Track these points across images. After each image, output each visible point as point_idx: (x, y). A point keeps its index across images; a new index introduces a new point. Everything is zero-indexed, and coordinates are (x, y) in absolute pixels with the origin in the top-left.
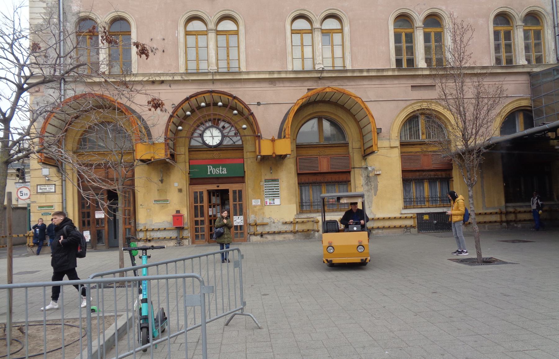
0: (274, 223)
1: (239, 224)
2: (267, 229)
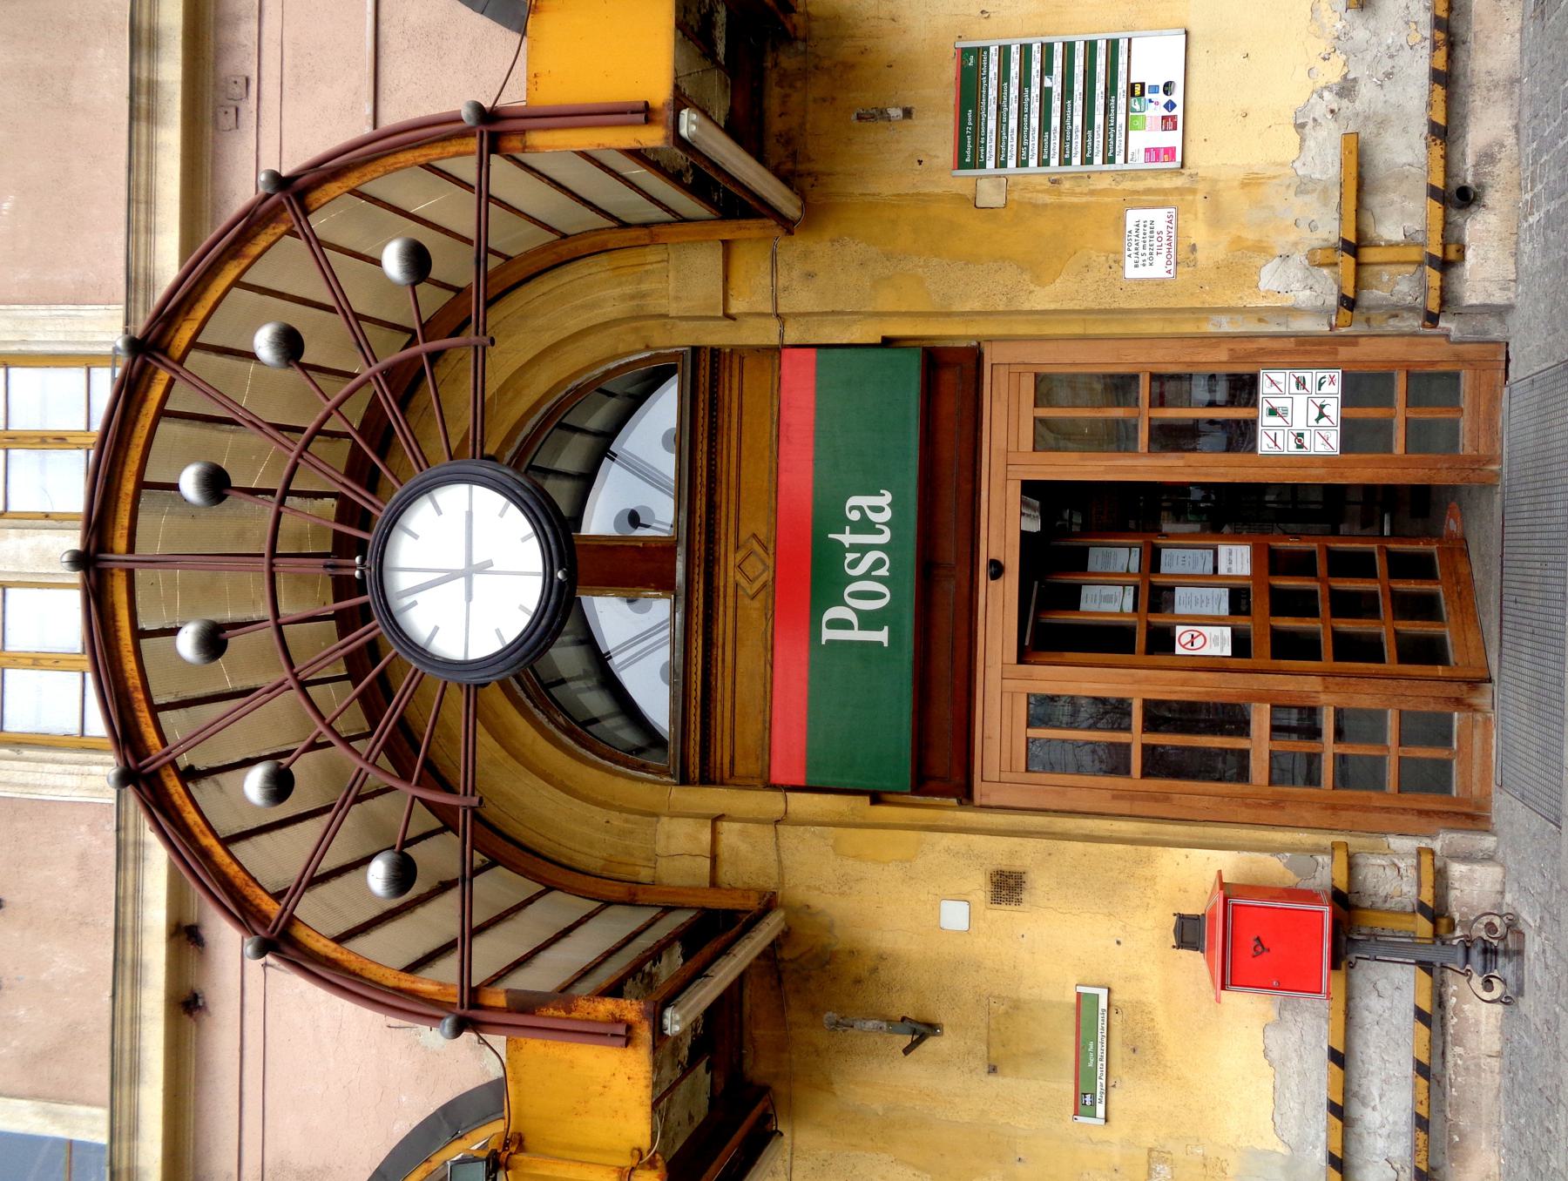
0: (1346, 89)
1: (1333, 410)
2: (1405, 151)
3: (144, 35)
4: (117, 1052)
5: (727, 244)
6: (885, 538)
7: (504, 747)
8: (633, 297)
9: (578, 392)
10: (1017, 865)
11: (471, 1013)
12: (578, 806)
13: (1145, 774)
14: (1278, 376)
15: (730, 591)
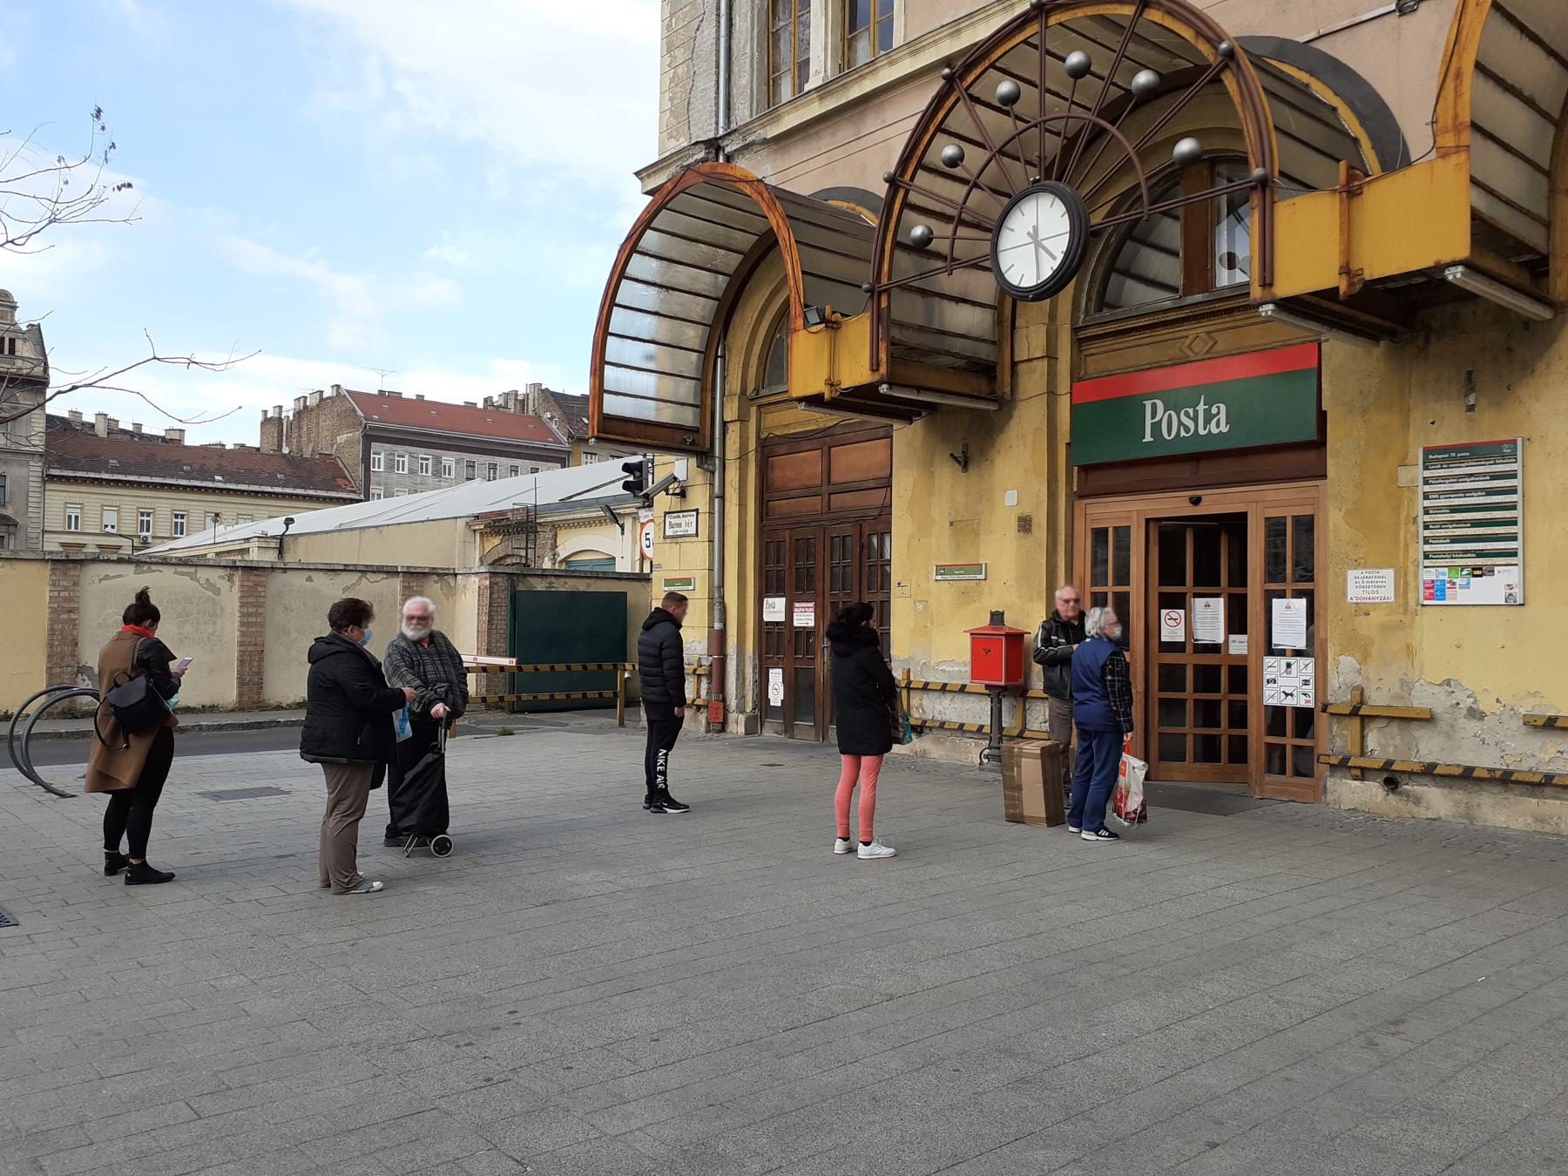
0: (1475, 714)
1: (1290, 702)
2: (1428, 747)
6: (1202, 432)
10: (1034, 529)
13: (1093, 593)
14: (1311, 668)
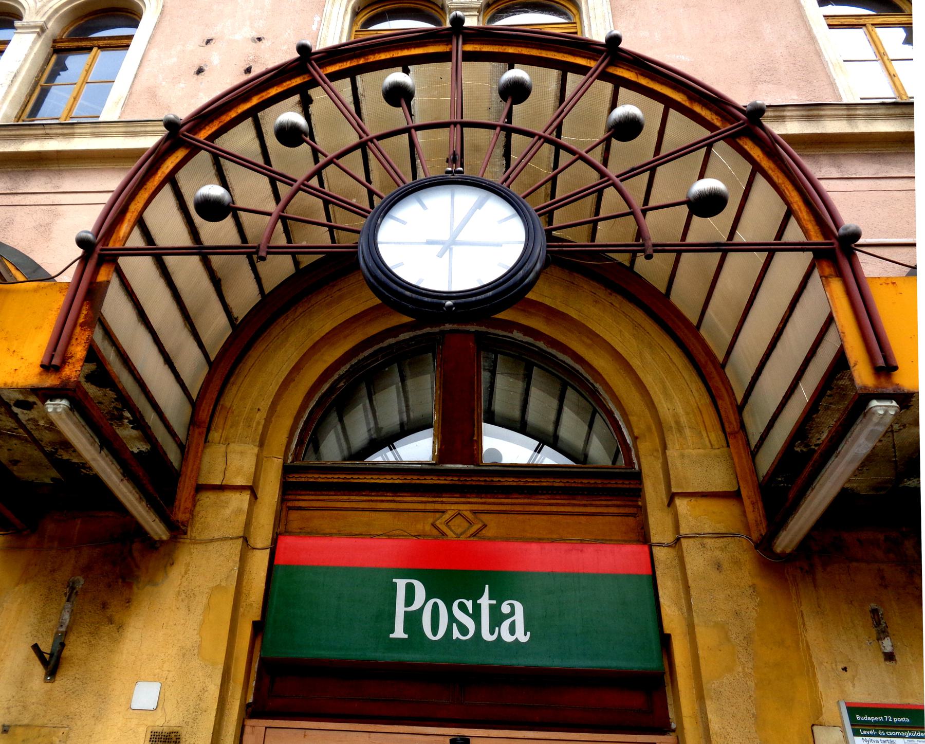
3: (815, 113)
4: (145, 123)
5: (735, 496)
6: (486, 636)
7: (323, 338)
8: (678, 423)
9: (594, 393)
11: (96, 256)
12: (273, 388)
15: (438, 507)
